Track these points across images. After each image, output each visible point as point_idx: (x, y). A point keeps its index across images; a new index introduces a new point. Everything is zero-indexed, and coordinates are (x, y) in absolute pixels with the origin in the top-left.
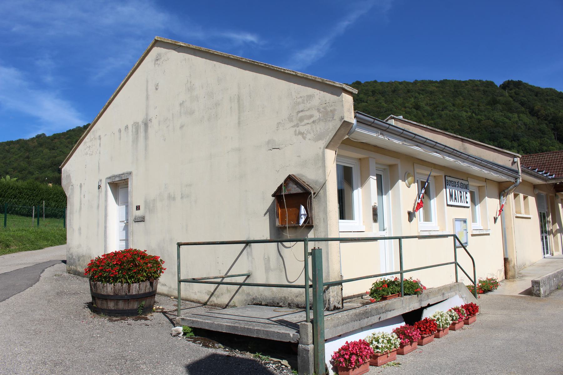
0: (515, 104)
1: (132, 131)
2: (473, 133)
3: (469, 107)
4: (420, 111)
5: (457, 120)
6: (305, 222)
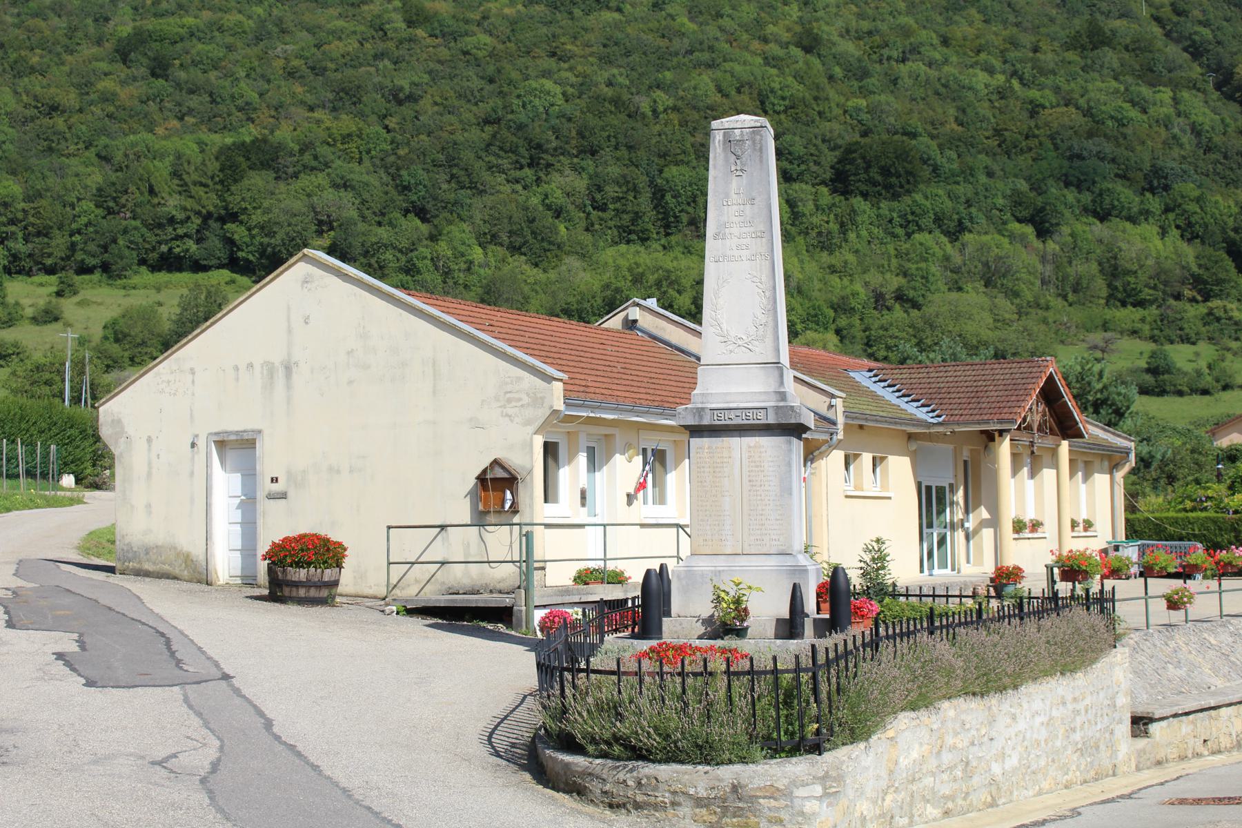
0: (1168, 49)
1: (262, 373)
2: (1008, 153)
3: (1002, 52)
4: (819, 56)
5: (954, 100)
6: (510, 507)
